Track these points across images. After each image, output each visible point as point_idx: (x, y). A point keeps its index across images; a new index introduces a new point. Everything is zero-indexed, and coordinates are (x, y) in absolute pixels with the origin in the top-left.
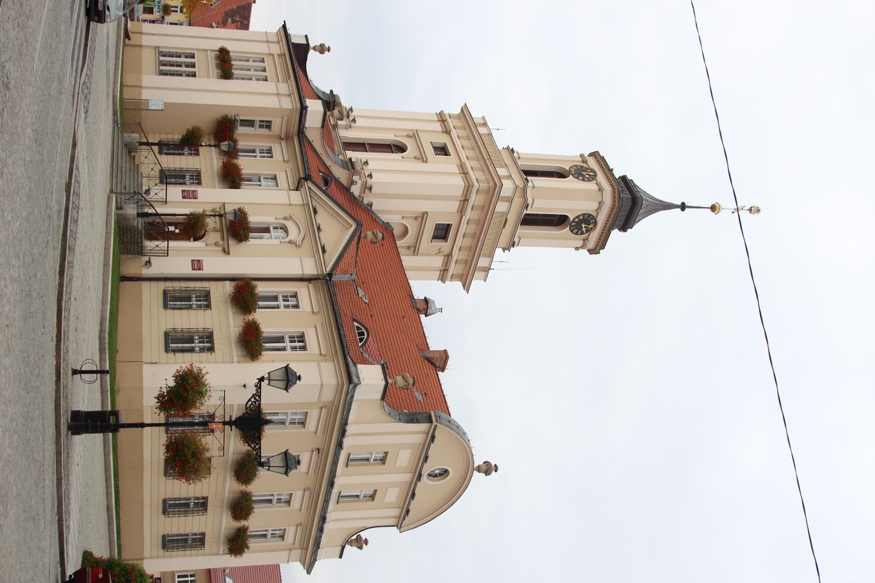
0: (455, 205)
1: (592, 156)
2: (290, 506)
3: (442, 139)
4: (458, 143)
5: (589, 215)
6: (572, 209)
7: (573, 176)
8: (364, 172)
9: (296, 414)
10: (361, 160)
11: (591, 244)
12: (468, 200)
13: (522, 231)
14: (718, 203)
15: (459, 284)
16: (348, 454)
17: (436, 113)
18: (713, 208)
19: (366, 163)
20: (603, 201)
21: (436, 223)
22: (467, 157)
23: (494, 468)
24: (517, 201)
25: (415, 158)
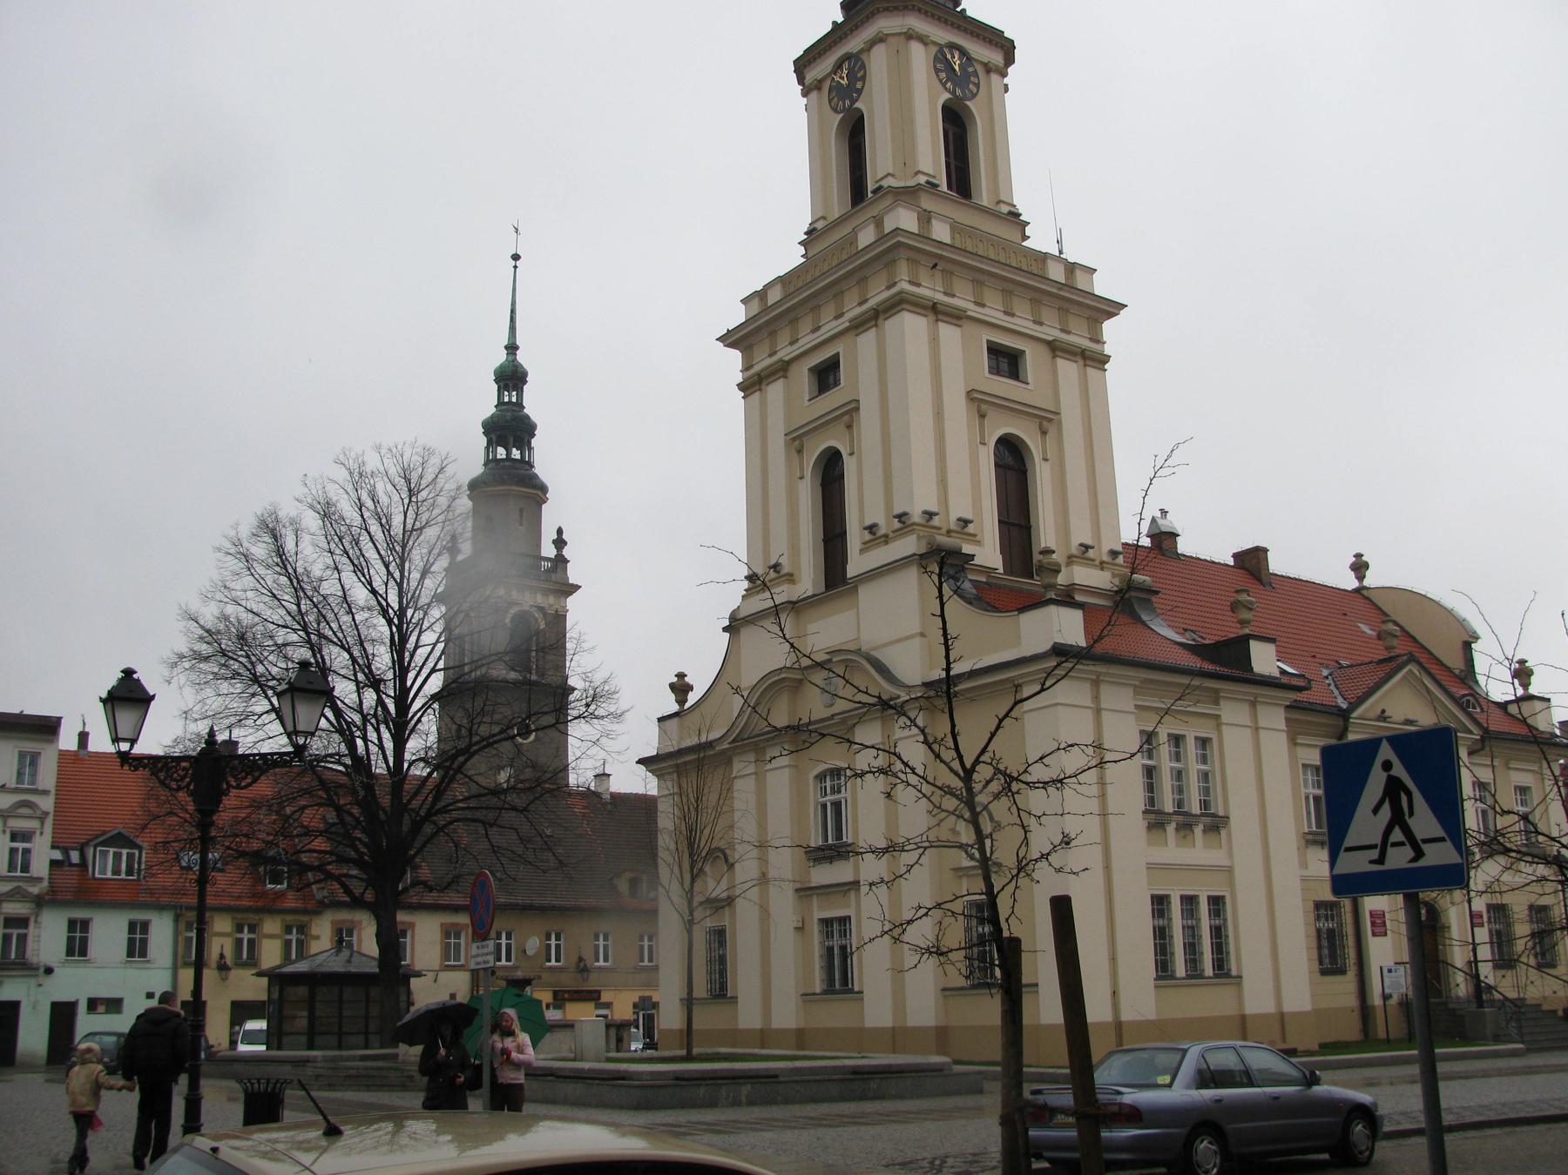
0: (947, 332)
3: (802, 376)
4: (806, 341)
5: (936, 59)
6: (927, 99)
7: (857, 100)
8: (894, 532)
9: (1306, 781)
10: (864, 543)
11: (997, 58)
12: (935, 304)
13: (984, 198)
15: (1109, 328)
19: (871, 528)
21: (987, 374)
22: (836, 318)
24: (926, 203)
25: (849, 427)
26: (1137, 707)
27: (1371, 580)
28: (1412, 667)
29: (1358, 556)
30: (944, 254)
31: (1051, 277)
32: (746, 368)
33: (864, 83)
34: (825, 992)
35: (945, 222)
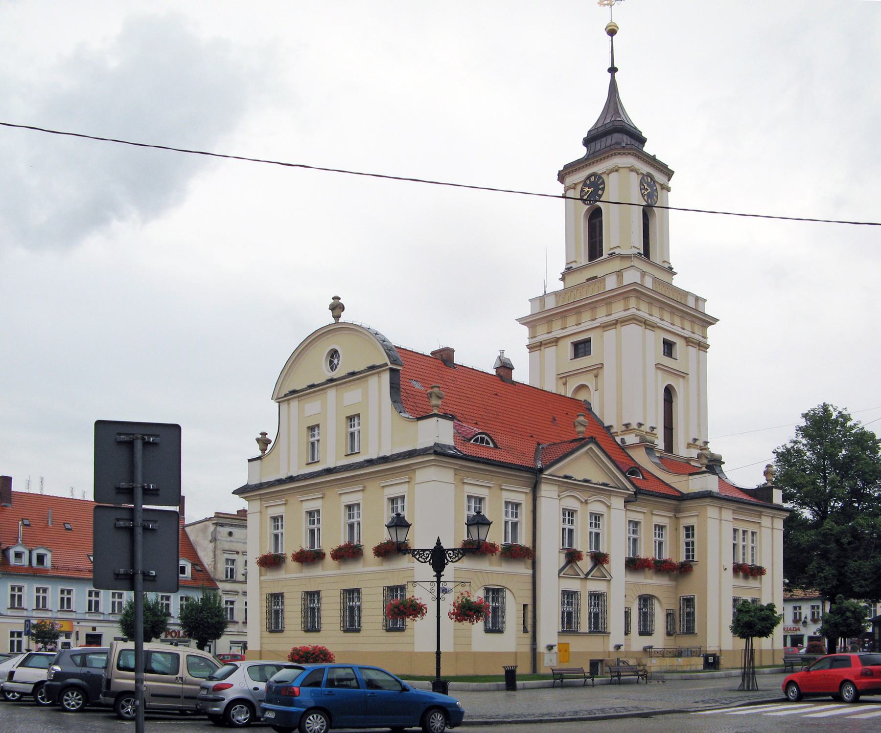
1: (564, 177)
2: (640, 522)
3: (567, 347)
9: (507, 512)
14: (605, 27)
15: (710, 329)
16: (346, 457)
17: (529, 352)
18: (612, 32)
20: (629, 167)
23: (337, 300)
25: (596, 376)
26: (733, 518)
27: (345, 317)
28: (591, 446)
29: (336, 298)
30: (706, 319)
31: (706, 313)
32: (532, 337)
33: (603, 192)
34: (590, 632)
35: (638, 271)
